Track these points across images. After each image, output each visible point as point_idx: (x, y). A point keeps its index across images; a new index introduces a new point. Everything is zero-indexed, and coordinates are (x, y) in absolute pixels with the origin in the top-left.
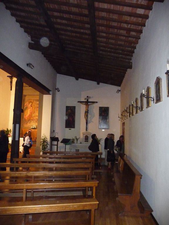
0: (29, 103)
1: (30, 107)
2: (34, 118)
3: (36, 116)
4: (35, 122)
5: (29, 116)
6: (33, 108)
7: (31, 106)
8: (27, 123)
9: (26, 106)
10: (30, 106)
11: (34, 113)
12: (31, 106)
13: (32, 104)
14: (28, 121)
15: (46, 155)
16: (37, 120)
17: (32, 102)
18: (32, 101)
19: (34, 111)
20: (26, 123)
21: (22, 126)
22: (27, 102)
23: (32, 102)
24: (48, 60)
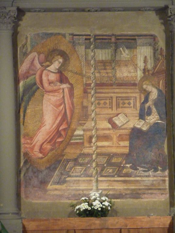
0: (49, 58)
1: (50, 83)
2: (86, 151)
3: (99, 138)
4: (92, 171)
5: (51, 140)
6: (71, 90)
7: (62, 79)
8: (44, 183)
9: (27, 75)
10: (53, 77)
11: (85, 116)
12: (62, 79)
13: (63, 65)
14: (52, 168)
15: (136, 201)
16: (103, 160)
17: (63, 54)
18: (63, 48)
19: (84, 108)
20: (35, 181)
21: (152, 55)
22: (34, 54)
23: (63, 54)
24: (112, 120)
